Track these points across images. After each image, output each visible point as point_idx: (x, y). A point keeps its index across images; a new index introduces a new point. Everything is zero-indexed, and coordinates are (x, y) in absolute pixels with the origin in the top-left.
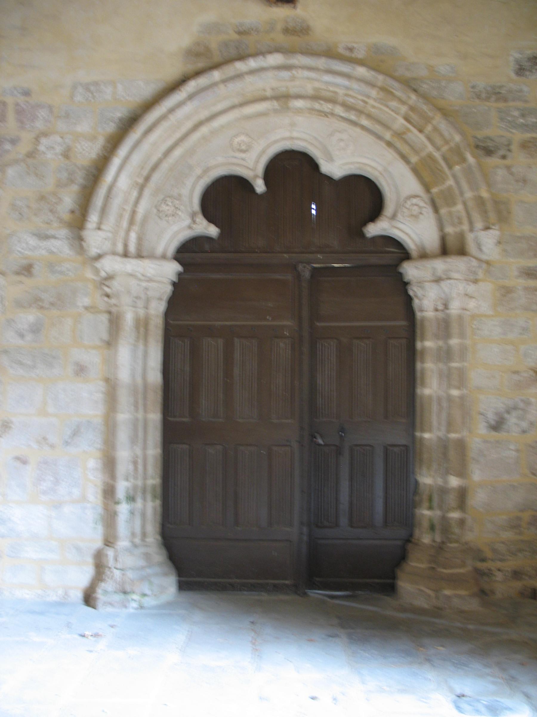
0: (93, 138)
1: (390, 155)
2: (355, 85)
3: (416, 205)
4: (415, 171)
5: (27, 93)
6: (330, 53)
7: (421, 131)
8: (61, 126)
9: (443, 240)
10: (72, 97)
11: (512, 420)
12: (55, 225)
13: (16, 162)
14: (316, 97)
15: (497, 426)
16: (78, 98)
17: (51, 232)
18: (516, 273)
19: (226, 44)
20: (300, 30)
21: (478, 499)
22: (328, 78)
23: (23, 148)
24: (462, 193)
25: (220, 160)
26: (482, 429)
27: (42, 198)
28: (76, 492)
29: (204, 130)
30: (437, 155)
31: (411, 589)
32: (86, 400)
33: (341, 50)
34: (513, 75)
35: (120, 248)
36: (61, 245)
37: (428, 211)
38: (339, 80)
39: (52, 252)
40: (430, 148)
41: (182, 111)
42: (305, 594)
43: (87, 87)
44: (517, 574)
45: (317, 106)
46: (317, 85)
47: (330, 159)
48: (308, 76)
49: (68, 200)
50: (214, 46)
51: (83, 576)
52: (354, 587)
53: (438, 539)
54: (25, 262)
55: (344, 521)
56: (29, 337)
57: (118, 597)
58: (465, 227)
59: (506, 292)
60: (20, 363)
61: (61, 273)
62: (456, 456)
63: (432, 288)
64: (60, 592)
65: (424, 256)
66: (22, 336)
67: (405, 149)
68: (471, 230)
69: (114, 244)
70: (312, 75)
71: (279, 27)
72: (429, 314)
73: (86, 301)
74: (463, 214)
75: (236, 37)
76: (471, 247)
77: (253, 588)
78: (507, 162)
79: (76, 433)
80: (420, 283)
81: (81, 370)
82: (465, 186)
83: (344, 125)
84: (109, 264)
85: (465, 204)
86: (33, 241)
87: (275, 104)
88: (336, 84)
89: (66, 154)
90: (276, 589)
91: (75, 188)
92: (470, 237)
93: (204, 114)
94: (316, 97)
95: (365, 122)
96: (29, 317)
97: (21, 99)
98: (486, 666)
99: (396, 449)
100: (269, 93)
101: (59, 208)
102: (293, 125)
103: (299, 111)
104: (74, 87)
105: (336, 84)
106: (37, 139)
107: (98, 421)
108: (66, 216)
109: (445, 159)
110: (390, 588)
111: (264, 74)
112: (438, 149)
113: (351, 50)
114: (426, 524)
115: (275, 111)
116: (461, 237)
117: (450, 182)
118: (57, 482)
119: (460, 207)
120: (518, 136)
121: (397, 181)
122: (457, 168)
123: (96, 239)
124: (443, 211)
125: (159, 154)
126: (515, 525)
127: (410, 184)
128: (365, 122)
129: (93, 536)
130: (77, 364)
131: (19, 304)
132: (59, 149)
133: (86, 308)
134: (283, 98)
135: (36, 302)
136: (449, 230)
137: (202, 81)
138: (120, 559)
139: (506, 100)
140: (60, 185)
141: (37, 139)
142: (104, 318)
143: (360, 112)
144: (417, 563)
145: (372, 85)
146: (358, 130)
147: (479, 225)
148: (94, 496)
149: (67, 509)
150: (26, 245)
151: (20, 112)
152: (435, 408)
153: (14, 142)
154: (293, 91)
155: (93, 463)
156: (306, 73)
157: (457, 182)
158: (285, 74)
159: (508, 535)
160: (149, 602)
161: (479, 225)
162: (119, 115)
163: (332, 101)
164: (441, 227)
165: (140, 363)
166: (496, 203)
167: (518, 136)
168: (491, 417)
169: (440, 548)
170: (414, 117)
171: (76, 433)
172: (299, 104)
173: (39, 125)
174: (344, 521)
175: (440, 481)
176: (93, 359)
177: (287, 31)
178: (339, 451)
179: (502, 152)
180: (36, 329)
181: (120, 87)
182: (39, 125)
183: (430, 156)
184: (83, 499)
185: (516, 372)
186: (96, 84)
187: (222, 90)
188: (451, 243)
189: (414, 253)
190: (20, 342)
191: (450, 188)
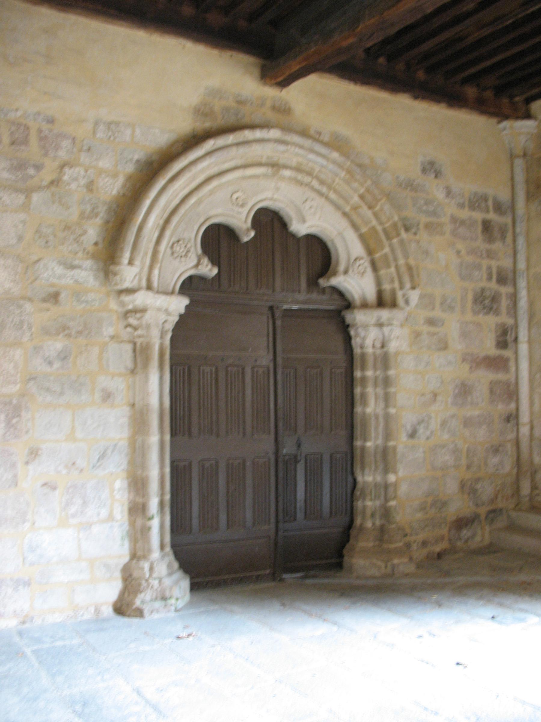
0: (115, 176)
1: (344, 224)
2: (331, 166)
3: (359, 266)
4: (362, 238)
5: (51, 121)
6: (304, 133)
7: (370, 207)
8: (84, 158)
9: (380, 294)
10: (94, 133)
11: (421, 430)
12: (80, 255)
13: (39, 188)
14: (298, 169)
15: (413, 435)
16: (99, 135)
17: (76, 262)
18: (422, 322)
19: (227, 109)
20: (284, 110)
21: (403, 489)
22: (312, 156)
23: (47, 176)
24: (396, 259)
25: (219, 211)
26: (404, 437)
27: (67, 228)
28: (104, 513)
29: (215, 183)
30: (379, 228)
31: (362, 562)
32: (114, 425)
33: (312, 132)
34: (420, 173)
35: (144, 283)
36: (86, 275)
37: (369, 270)
38: (320, 160)
39: (76, 281)
40: (374, 222)
41: (199, 164)
42: (281, 580)
43: (109, 124)
44: (424, 544)
45: (300, 177)
46: (300, 159)
47: (303, 220)
48: (294, 153)
49: (93, 232)
50: (217, 108)
51: (111, 591)
52: (307, 568)
53: (378, 523)
54: (52, 290)
55: (300, 515)
56: (57, 365)
57: (158, 604)
58: (396, 285)
59: (417, 335)
60: (48, 390)
61: (87, 302)
62: (386, 458)
63: (368, 331)
64: (92, 610)
65: (365, 305)
66: (50, 363)
67: (358, 221)
68: (402, 288)
69: (140, 280)
70: (301, 152)
71: (269, 103)
72: (369, 350)
73: (111, 331)
74: (395, 275)
75: (234, 105)
76: (400, 301)
77: (241, 581)
78: (417, 237)
79: (102, 456)
80: (366, 327)
81: (107, 396)
82: (400, 255)
83: (313, 195)
84: (142, 298)
85: (397, 267)
86: (59, 270)
87: (270, 170)
88: (315, 161)
89: (90, 186)
90: (258, 579)
91: (99, 221)
92: (400, 294)
93: (215, 170)
94: (298, 169)
95: (332, 196)
96: (57, 345)
97: (45, 127)
98: (481, 598)
99: (338, 456)
100: (264, 160)
101: (84, 238)
102: (277, 189)
103: (283, 178)
104: (97, 123)
105: (315, 161)
106: (62, 167)
107: (124, 444)
108: (90, 248)
109: (385, 231)
110: (339, 566)
111: (264, 145)
112: (381, 223)
113: (320, 134)
114: (369, 512)
115: (265, 176)
116: (393, 293)
117: (387, 250)
118: (85, 503)
119: (393, 269)
120: (424, 219)
121: (347, 245)
122: (395, 241)
123: (129, 274)
124: (382, 272)
125: (177, 201)
126: (423, 508)
127: (357, 249)
128: (332, 196)
129: (120, 551)
130: (103, 390)
131: (46, 331)
132: (83, 182)
133: (112, 338)
134: (275, 166)
135: (63, 329)
136: (387, 287)
137: (220, 141)
138: (156, 569)
139: (416, 191)
140: (83, 216)
141: (62, 167)
142: (129, 347)
143: (330, 187)
144: (363, 543)
145: (340, 166)
146: (323, 200)
147: (408, 285)
148: (120, 513)
149: (95, 529)
150: (52, 273)
151: (42, 139)
152: (373, 423)
153: (38, 167)
154: (282, 161)
155: (120, 484)
156: (297, 150)
157: (393, 250)
158: (282, 148)
159: (419, 515)
160: (180, 604)
161: (408, 285)
162: (136, 157)
163: (309, 173)
164: (378, 282)
165: (155, 388)
166: (410, 268)
167: (424, 219)
168: (409, 428)
169: (382, 530)
170: (369, 197)
171: (102, 456)
172: (287, 173)
173: (63, 154)
174: (300, 515)
175: (379, 478)
176: (119, 385)
177: (274, 108)
178: (296, 461)
179: (414, 230)
180: (64, 356)
181: (138, 131)
182: (63, 154)
183: (373, 229)
184: (111, 518)
185: (423, 395)
186: (117, 124)
187: (234, 151)
188: (387, 297)
189: (358, 302)
190: (46, 369)
191: (386, 255)
